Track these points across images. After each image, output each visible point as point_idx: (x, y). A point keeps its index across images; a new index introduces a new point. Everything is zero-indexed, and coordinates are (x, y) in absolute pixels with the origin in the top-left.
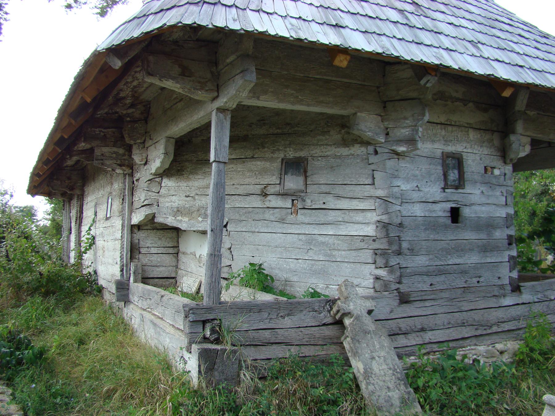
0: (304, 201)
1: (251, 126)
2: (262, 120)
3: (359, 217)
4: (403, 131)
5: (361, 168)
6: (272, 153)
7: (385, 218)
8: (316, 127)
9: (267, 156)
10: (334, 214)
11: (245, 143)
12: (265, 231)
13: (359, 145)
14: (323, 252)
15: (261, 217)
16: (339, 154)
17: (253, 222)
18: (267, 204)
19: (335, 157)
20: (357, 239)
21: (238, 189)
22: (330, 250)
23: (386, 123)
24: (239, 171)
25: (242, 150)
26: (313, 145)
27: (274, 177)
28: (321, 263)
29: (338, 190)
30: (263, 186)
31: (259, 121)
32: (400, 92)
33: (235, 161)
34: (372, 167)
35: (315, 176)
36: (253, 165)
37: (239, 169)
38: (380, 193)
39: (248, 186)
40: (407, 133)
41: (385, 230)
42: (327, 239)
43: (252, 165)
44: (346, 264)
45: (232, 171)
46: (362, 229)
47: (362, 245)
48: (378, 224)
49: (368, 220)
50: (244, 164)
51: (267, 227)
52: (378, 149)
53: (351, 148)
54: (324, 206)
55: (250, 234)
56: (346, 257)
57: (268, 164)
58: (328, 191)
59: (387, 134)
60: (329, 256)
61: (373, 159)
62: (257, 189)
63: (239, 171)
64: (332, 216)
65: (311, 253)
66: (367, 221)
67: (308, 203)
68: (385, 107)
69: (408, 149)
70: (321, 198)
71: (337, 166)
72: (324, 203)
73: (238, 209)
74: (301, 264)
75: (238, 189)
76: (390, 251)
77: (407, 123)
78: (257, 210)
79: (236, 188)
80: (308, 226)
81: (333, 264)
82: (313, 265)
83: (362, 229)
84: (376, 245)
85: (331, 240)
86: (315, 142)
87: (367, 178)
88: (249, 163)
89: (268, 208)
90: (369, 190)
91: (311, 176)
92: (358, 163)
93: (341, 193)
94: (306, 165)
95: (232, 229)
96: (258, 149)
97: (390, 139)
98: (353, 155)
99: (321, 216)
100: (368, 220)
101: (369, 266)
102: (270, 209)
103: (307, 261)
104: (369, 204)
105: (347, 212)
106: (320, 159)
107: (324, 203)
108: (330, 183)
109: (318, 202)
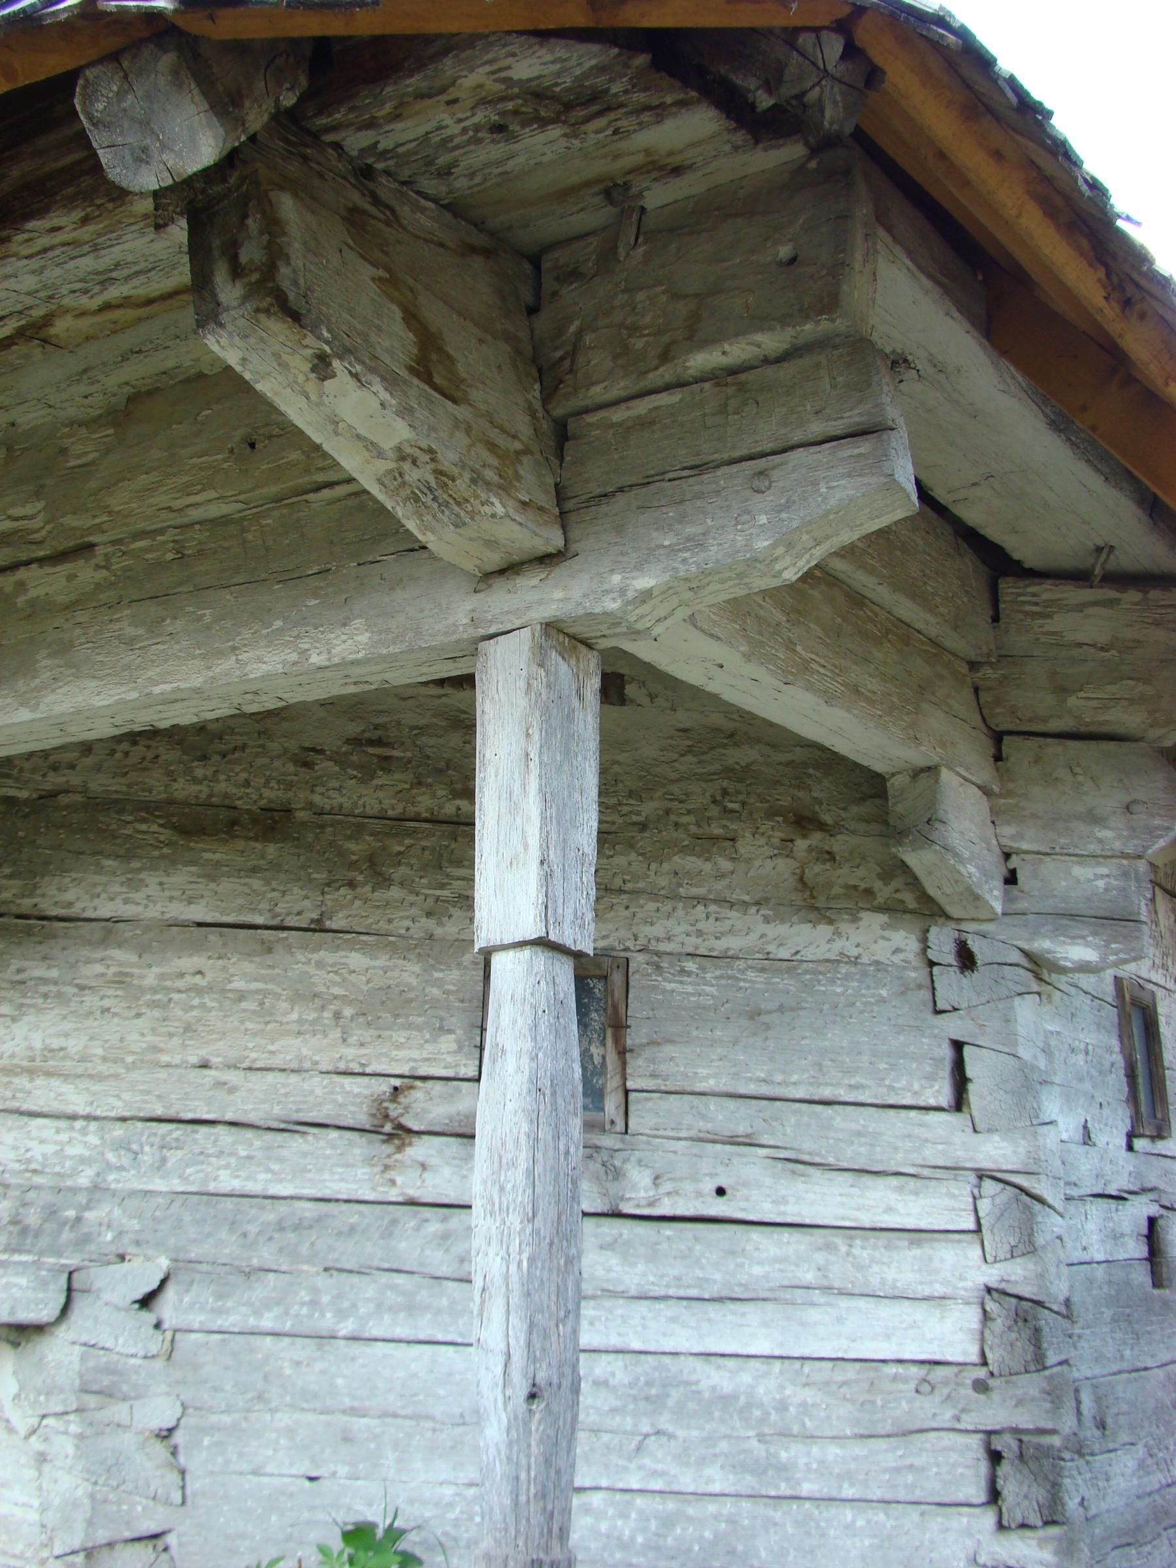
0: (617, 1174)
1: (307, 765)
2: (371, 742)
3: (901, 1267)
4: (1082, 872)
5: (900, 1029)
6: (429, 914)
7: (1018, 1274)
8: (668, 812)
9: (400, 925)
10: (774, 1251)
11: (271, 849)
12: (399, 1332)
13: (883, 918)
14: (723, 1446)
15: (372, 1250)
16: (784, 953)
17: (322, 1281)
18: (408, 1184)
19: (768, 962)
20: (895, 1378)
21: (233, 1090)
22: (761, 1438)
23: (1007, 831)
24: (241, 996)
25: (256, 883)
26: (654, 896)
27: (447, 1043)
28: (712, 1508)
29: (795, 1130)
30: (384, 1087)
31: (356, 742)
32: (1072, 701)
33: (213, 935)
34: (954, 1027)
35: (668, 1049)
36: (320, 965)
37: (239, 984)
38: (996, 1151)
39: (294, 1079)
40: (1101, 884)
41: (1027, 1333)
42: (746, 1378)
43: (313, 964)
44: (848, 1514)
45: (199, 991)
46: (914, 1325)
47: (929, 1409)
48: (990, 1306)
49: (945, 1283)
50: (269, 960)
51: (412, 1309)
52: (975, 945)
53: (844, 927)
54: (718, 1208)
55: (303, 1350)
56: (848, 1476)
57: (408, 972)
58: (742, 1129)
59: (1011, 879)
60: (759, 1469)
61: (952, 985)
62: (354, 1099)
63: (241, 996)
64: (764, 1259)
65: (659, 1457)
66: (939, 1290)
67: (638, 1189)
68: (998, 758)
69: (1103, 958)
70: (705, 1166)
71: (781, 1009)
72: (721, 1192)
73: (229, 1203)
74: (600, 1515)
75: (233, 1090)
76: (1056, 1441)
77: (1100, 841)
78: (352, 1215)
79: (221, 1084)
80: (643, 1307)
81: (778, 1516)
82: (668, 1522)
83: (914, 1325)
84: (997, 1413)
85: (767, 1386)
86: (663, 882)
87: (931, 1078)
88: (300, 956)
89: (412, 1203)
90: (946, 1137)
91: (648, 1053)
92: (882, 1000)
93: (808, 1146)
94: (618, 993)
95: (197, 1319)
96: (352, 884)
97: (1023, 905)
98: (855, 961)
99: (708, 1259)
100: (945, 1283)
101: (962, 1519)
102: (427, 1212)
103: (639, 1501)
104: (948, 1202)
105: (839, 1240)
106: (690, 965)
107: (721, 1192)
108: (751, 1089)
109: (689, 1187)
